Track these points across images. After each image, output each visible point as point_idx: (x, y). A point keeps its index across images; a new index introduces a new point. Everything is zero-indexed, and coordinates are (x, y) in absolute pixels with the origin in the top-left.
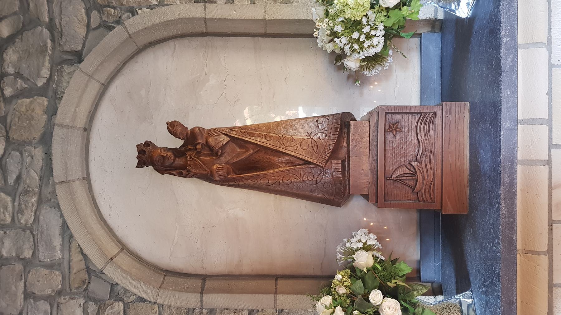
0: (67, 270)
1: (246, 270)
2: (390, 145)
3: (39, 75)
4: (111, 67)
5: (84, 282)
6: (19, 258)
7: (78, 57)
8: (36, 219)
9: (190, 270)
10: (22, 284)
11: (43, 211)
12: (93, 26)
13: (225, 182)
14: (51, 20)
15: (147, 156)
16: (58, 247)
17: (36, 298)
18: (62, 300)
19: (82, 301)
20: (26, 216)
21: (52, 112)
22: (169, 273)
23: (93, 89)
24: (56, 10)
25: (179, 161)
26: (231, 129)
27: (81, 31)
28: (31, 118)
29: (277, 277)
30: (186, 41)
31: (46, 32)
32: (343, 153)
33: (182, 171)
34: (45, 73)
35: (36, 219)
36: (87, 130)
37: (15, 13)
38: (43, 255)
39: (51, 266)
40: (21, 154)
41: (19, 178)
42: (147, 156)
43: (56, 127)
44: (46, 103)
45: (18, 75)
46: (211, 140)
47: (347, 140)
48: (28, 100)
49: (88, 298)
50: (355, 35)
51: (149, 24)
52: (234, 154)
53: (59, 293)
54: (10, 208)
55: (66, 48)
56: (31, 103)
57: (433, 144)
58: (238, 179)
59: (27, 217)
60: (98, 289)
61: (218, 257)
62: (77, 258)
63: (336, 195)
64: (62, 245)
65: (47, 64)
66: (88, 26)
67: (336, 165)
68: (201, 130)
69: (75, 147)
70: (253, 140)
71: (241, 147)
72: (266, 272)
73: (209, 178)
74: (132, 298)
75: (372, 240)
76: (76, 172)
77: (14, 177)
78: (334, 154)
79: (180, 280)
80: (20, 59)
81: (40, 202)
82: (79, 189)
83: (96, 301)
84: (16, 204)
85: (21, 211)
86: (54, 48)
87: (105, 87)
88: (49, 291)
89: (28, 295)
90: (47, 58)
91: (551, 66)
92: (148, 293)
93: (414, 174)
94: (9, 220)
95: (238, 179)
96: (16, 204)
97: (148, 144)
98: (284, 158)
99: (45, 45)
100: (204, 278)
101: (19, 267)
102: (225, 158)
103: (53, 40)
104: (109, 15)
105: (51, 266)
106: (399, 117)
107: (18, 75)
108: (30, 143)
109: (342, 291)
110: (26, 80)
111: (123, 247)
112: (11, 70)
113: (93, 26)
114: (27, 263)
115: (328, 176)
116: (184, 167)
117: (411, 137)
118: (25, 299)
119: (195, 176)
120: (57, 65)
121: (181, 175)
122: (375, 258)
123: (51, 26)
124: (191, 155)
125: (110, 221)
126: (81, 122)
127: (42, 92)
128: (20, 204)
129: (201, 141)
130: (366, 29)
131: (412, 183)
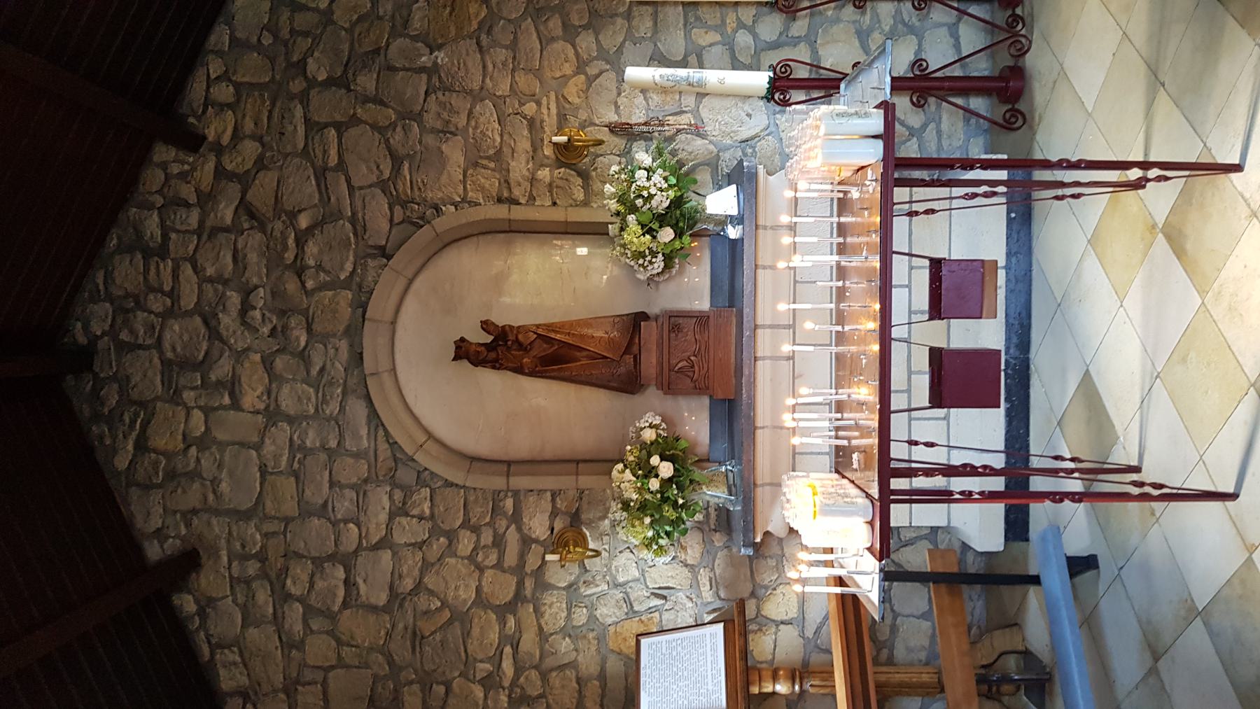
0: (373, 459)
1: (548, 455)
2: (673, 342)
3: (342, 268)
4: (418, 263)
5: (391, 469)
6: (324, 448)
7: (385, 253)
8: (342, 409)
9: (496, 457)
10: (327, 472)
11: (350, 402)
12: (396, 221)
13: (533, 374)
14: (354, 214)
15: (463, 351)
16: (365, 437)
17: (342, 487)
18: (368, 487)
19: (388, 489)
20: (331, 407)
21: (361, 306)
22: (474, 459)
23: (402, 283)
24: (359, 203)
25: (493, 355)
26: (538, 326)
27: (385, 226)
28: (335, 311)
29: (578, 462)
30: (490, 237)
31: (348, 226)
32: (635, 349)
33: (496, 365)
34: (349, 267)
35: (342, 409)
36: (393, 323)
37: (315, 205)
38: (349, 444)
39: (357, 456)
40: (325, 346)
41: (322, 369)
42: (463, 351)
43: (1002, 448)
44: (350, 296)
45: (319, 267)
46: (520, 337)
47: (952, 167)
48: (330, 293)
49: (395, 485)
50: (641, 261)
51: (455, 224)
52: (540, 350)
53: (366, 481)
54: (313, 399)
55: (370, 243)
56: (334, 296)
57: (707, 343)
58: (546, 371)
59: (333, 408)
60: (406, 476)
61: (522, 445)
62: (383, 446)
63: (630, 384)
64: (369, 433)
65: (351, 258)
66: (391, 220)
67: (629, 359)
68: (511, 327)
69: (383, 341)
70: (558, 337)
71: (547, 343)
72: (567, 457)
73: (519, 370)
74: (440, 484)
75: (657, 420)
76: (384, 364)
77: (318, 368)
78: (627, 350)
79: (487, 465)
80: (321, 252)
81: (344, 393)
82: (387, 379)
83: (401, 487)
84: (320, 395)
85: (325, 401)
86: (357, 243)
87: (411, 282)
88: (354, 480)
89: (332, 484)
90: (351, 253)
91: (795, 282)
92: (457, 476)
93: (693, 367)
94: (312, 411)
95: (546, 371)
96: (320, 395)
97: (462, 340)
98: (585, 353)
99: (349, 239)
100: (509, 463)
101: (323, 457)
102: (534, 353)
103: (355, 234)
104: (412, 210)
105: (357, 456)
106: (681, 321)
107: (319, 267)
108: (334, 335)
109: (631, 458)
110: (327, 272)
111: (430, 436)
112: (312, 263)
113: (396, 221)
114: (331, 453)
115: (622, 370)
116: (496, 360)
117: (690, 337)
118: (331, 487)
119: (506, 368)
120: (360, 260)
121: (494, 368)
122: (658, 435)
123: (353, 220)
124: (501, 349)
125: (416, 411)
126: (388, 316)
127: (346, 285)
128: (324, 395)
129: (511, 337)
130: (649, 258)
131: (691, 374)
